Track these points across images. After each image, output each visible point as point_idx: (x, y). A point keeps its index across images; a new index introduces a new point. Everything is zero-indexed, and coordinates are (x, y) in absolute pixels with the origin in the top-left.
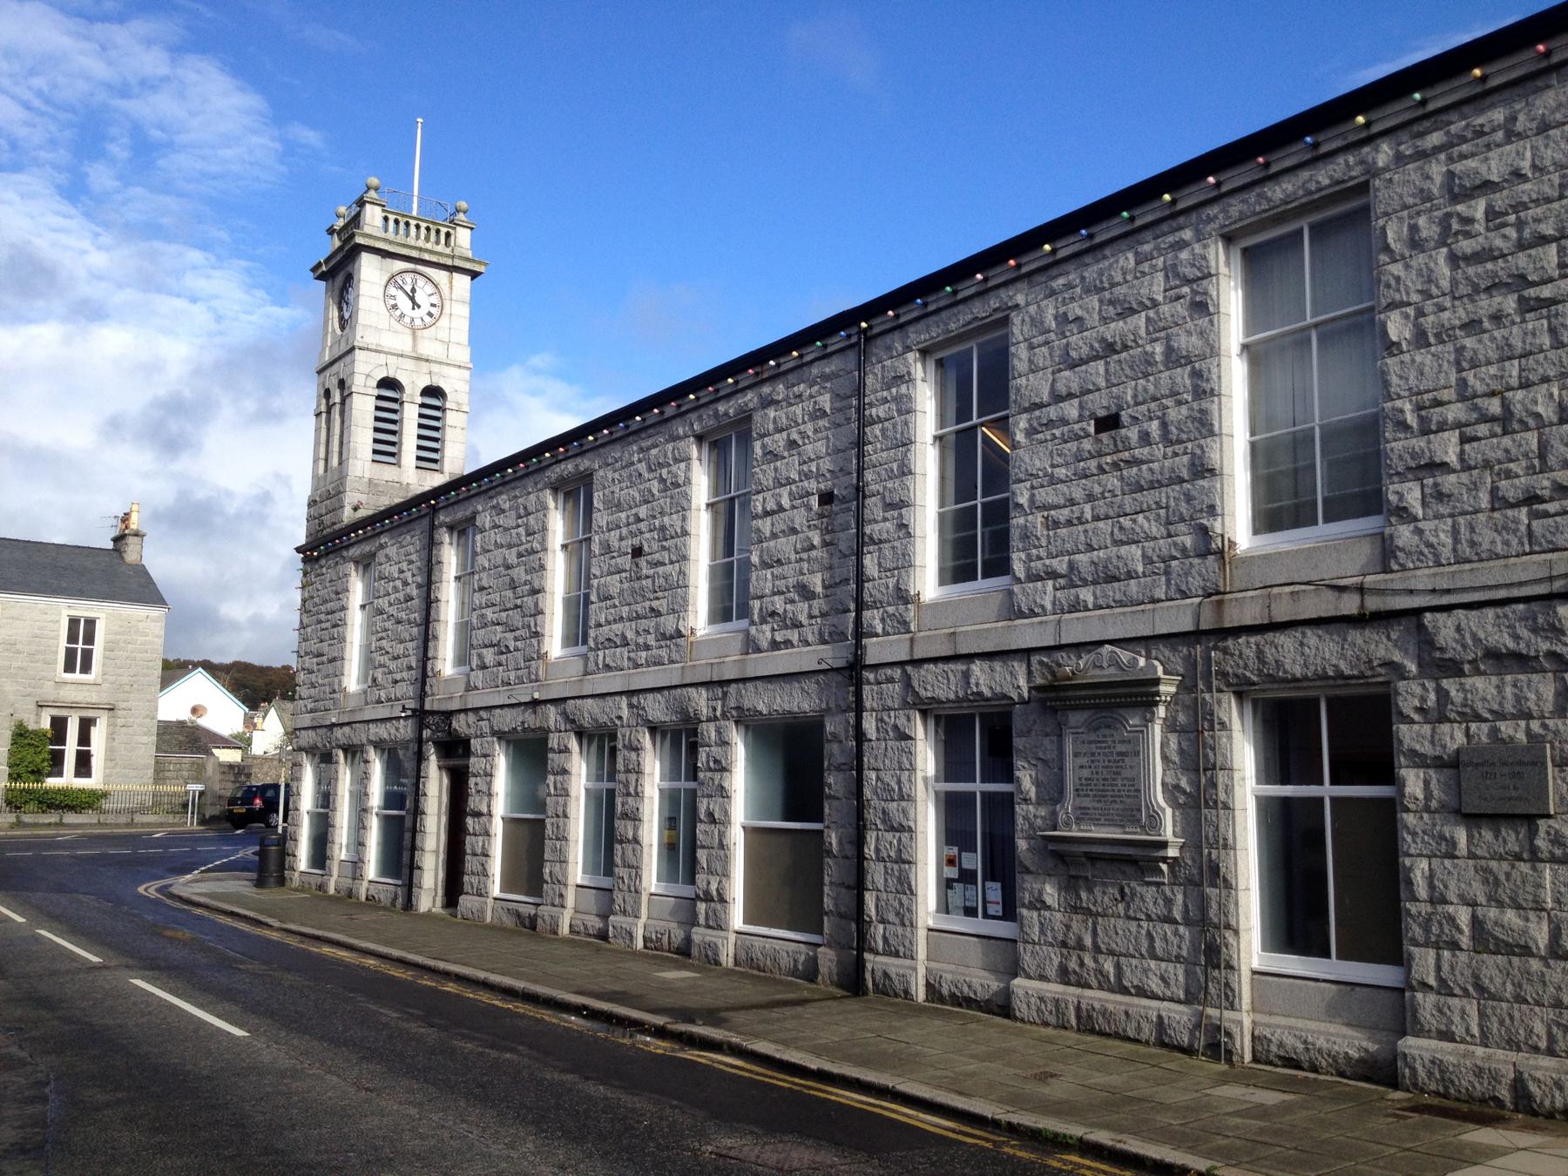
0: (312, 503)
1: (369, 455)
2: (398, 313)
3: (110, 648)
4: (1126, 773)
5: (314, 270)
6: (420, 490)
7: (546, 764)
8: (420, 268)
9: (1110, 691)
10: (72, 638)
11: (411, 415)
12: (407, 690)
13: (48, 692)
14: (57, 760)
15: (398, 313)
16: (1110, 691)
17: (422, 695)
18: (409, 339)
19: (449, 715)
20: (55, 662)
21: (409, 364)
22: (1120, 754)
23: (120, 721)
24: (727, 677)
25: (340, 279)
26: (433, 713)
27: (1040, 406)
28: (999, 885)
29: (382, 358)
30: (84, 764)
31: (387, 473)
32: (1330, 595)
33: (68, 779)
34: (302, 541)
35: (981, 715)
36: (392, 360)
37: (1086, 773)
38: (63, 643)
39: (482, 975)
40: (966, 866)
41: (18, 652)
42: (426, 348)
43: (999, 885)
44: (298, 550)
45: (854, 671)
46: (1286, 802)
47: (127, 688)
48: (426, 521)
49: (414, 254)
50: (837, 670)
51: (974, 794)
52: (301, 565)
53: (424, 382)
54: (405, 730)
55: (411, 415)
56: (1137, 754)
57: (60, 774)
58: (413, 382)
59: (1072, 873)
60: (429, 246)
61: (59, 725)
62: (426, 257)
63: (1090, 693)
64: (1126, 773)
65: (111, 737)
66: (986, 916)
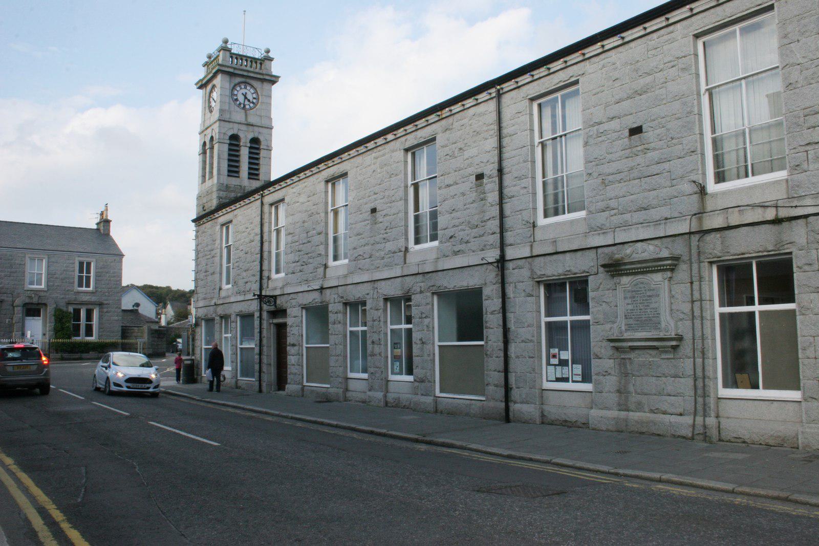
0: (199, 198)
1: (226, 173)
2: (238, 103)
3: (97, 275)
4: (652, 306)
5: (196, 84)
6: (250, 189)
7: (328, 319)
8: (248, 81)
9: (644, 265)
10: (81, 271)
11: (244, 153)
12: (256, 287)
13: (71, 297)
14: (77, 328)
15: (238, 103)
16: (644, 265)
17: (261, 289)
18: (244, 116)
19: (275, 297)
20: (73, 283)
21: (244, 128)
22: (650, 296)
23: (105, 310)
24: (427, 270)
25: (209, 87)
26: (266, 296)
27: (600, 123)
28: (580, 366)
29: (231, 125)
30: (89, 331)
31: (233, 181)
32: (760, 210)
33: (82, 338)
34: (195, 217)
35: (571, 283)
36: (236, 126)
37: (630, 307)
38: (77, 273)
39: (348, 425)
40: (562, 357)
41: (56, 278)
42: (251, 120)
43: (580, 366)
44: (194, 221)
45: (502, 262)
46: (732, 315)
47: (107, 294)
48: (259, 201)
49: (245, 74)
50: (491, 263)
51: (567, 321)
52: (195, 229)
53: (251, 136)
54: (254, 306)
55: (244, 153)
56: (658, 296)
57: (79, 335)
58: (246, 137)
59: (623, 357)
60: (252, 70)
61: (77, 312)
62: (252, 75)
63: (639, 266)
64: (652, 306)
65: (101, 317)
66: (573, 381)
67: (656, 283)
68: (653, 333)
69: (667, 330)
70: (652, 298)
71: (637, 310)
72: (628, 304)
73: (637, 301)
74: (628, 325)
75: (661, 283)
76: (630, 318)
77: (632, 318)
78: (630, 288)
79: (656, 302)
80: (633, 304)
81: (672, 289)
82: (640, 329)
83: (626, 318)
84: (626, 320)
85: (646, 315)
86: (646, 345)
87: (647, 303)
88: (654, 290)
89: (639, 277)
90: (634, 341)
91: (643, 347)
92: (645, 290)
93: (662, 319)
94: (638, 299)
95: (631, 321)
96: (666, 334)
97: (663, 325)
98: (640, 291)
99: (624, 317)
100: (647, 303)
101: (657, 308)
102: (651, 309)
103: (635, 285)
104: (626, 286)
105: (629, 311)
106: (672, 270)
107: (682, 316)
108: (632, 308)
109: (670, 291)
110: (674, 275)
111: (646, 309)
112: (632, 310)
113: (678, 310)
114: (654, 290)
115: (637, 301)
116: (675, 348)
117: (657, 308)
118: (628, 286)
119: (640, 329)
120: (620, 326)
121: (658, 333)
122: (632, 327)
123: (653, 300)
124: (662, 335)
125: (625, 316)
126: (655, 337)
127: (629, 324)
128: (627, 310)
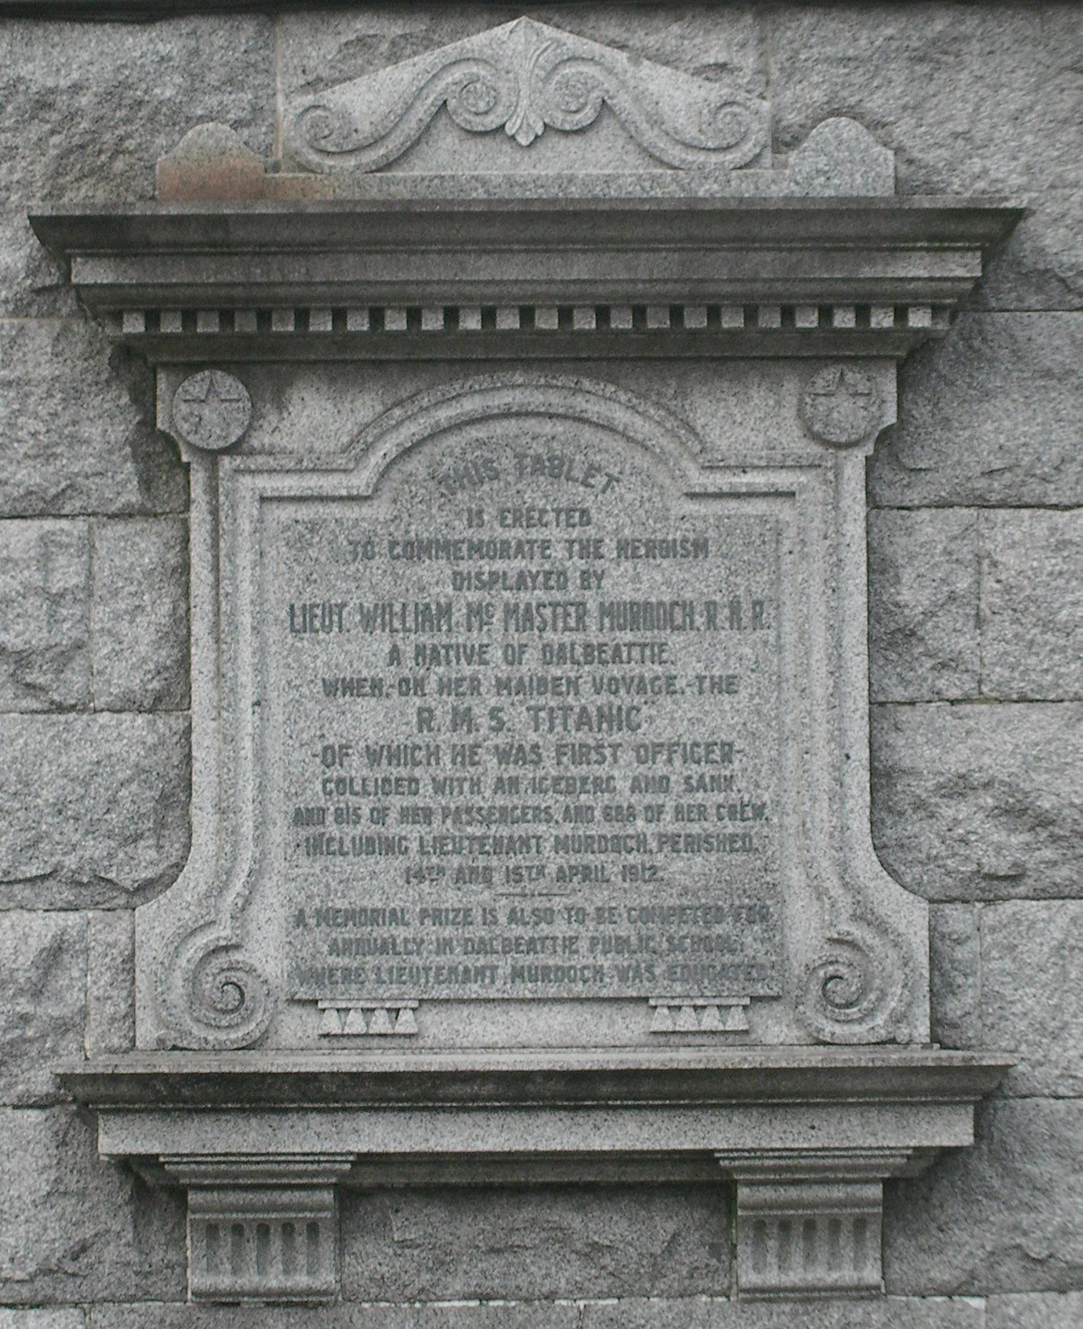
22: (636, 614)
23: (45, 484)
37: (369, 722)
56: (753, 614)
64: (668, 720)
67: (722, 481)
68: (332, 1023)
69: (840, 991)
70: (676, 640)
71: (466, 755)
72: (352, 687)
73: (477, 654)
74: (327, 917)
75: (783, 480)
76: (369, 846)
77: (391, 847)
78: (380, 510)
79: (727, 685)
80: (409, 686)
81: (899, 547)
82: (504, 965)
83: (316, 847)
84: (310, 866)
85: (581, 814)
86: (599, 1143)
87: (614, 686)
88: (700, 547)
89: (471, 405)
90: (464, 1106)
91: (611, 1174)
92: (591, 549)
93: (796, 876)
94: (496, 633)
95: (377, 883)
96: (830, 1029)
97: (804, 931)
98: (503, 550)
99: (279, 832)
100: (614, 686)
101: (728, 751)
102: (647, 752)
103: (448, 484)
104: (329, 484)
105: (356, 767)
106: (913, 360)
107: (1000, 846)
108: (403, 732)
109: (880, 568)
110: (921, 412)
111: (581, 754)
112: (395, 755)
113: (959, 787)
114: (700, 547)
115: (477, 654)
116: (915, 1189)
117: (728, 751)
118: (360, 481)
119: (504, 965)
120: (223, 932)
121: (736, 1021)
122: (386, 947)
123: (687, 655)
124: (779, 1039)
125: (303, 818)
126: (684, 1058)
127: (352, 916)
128: (333, 756)
